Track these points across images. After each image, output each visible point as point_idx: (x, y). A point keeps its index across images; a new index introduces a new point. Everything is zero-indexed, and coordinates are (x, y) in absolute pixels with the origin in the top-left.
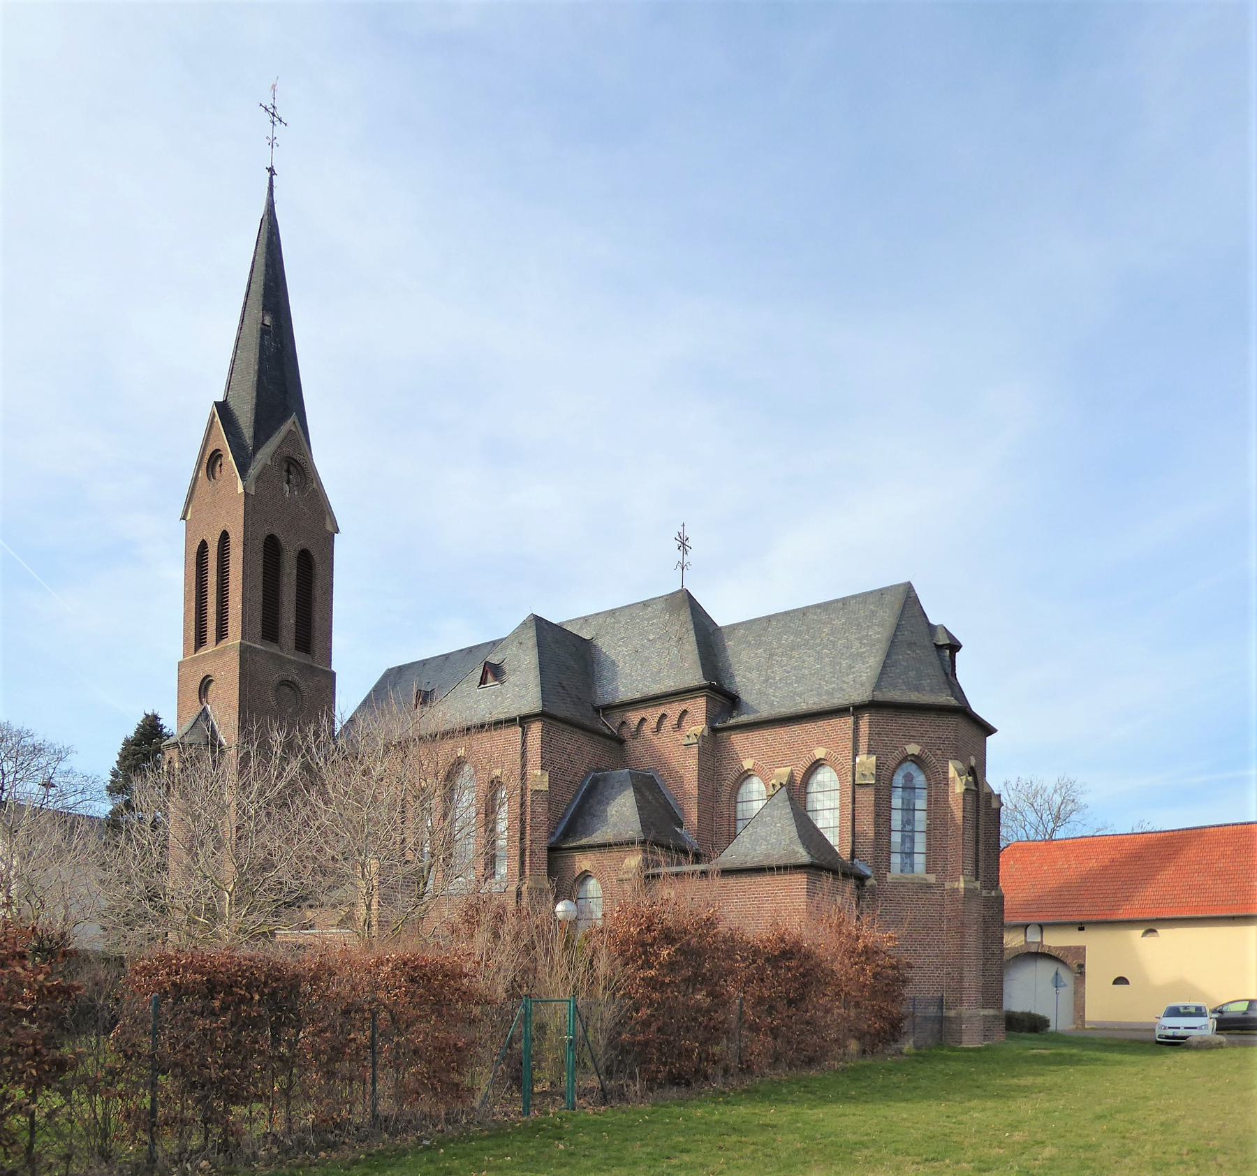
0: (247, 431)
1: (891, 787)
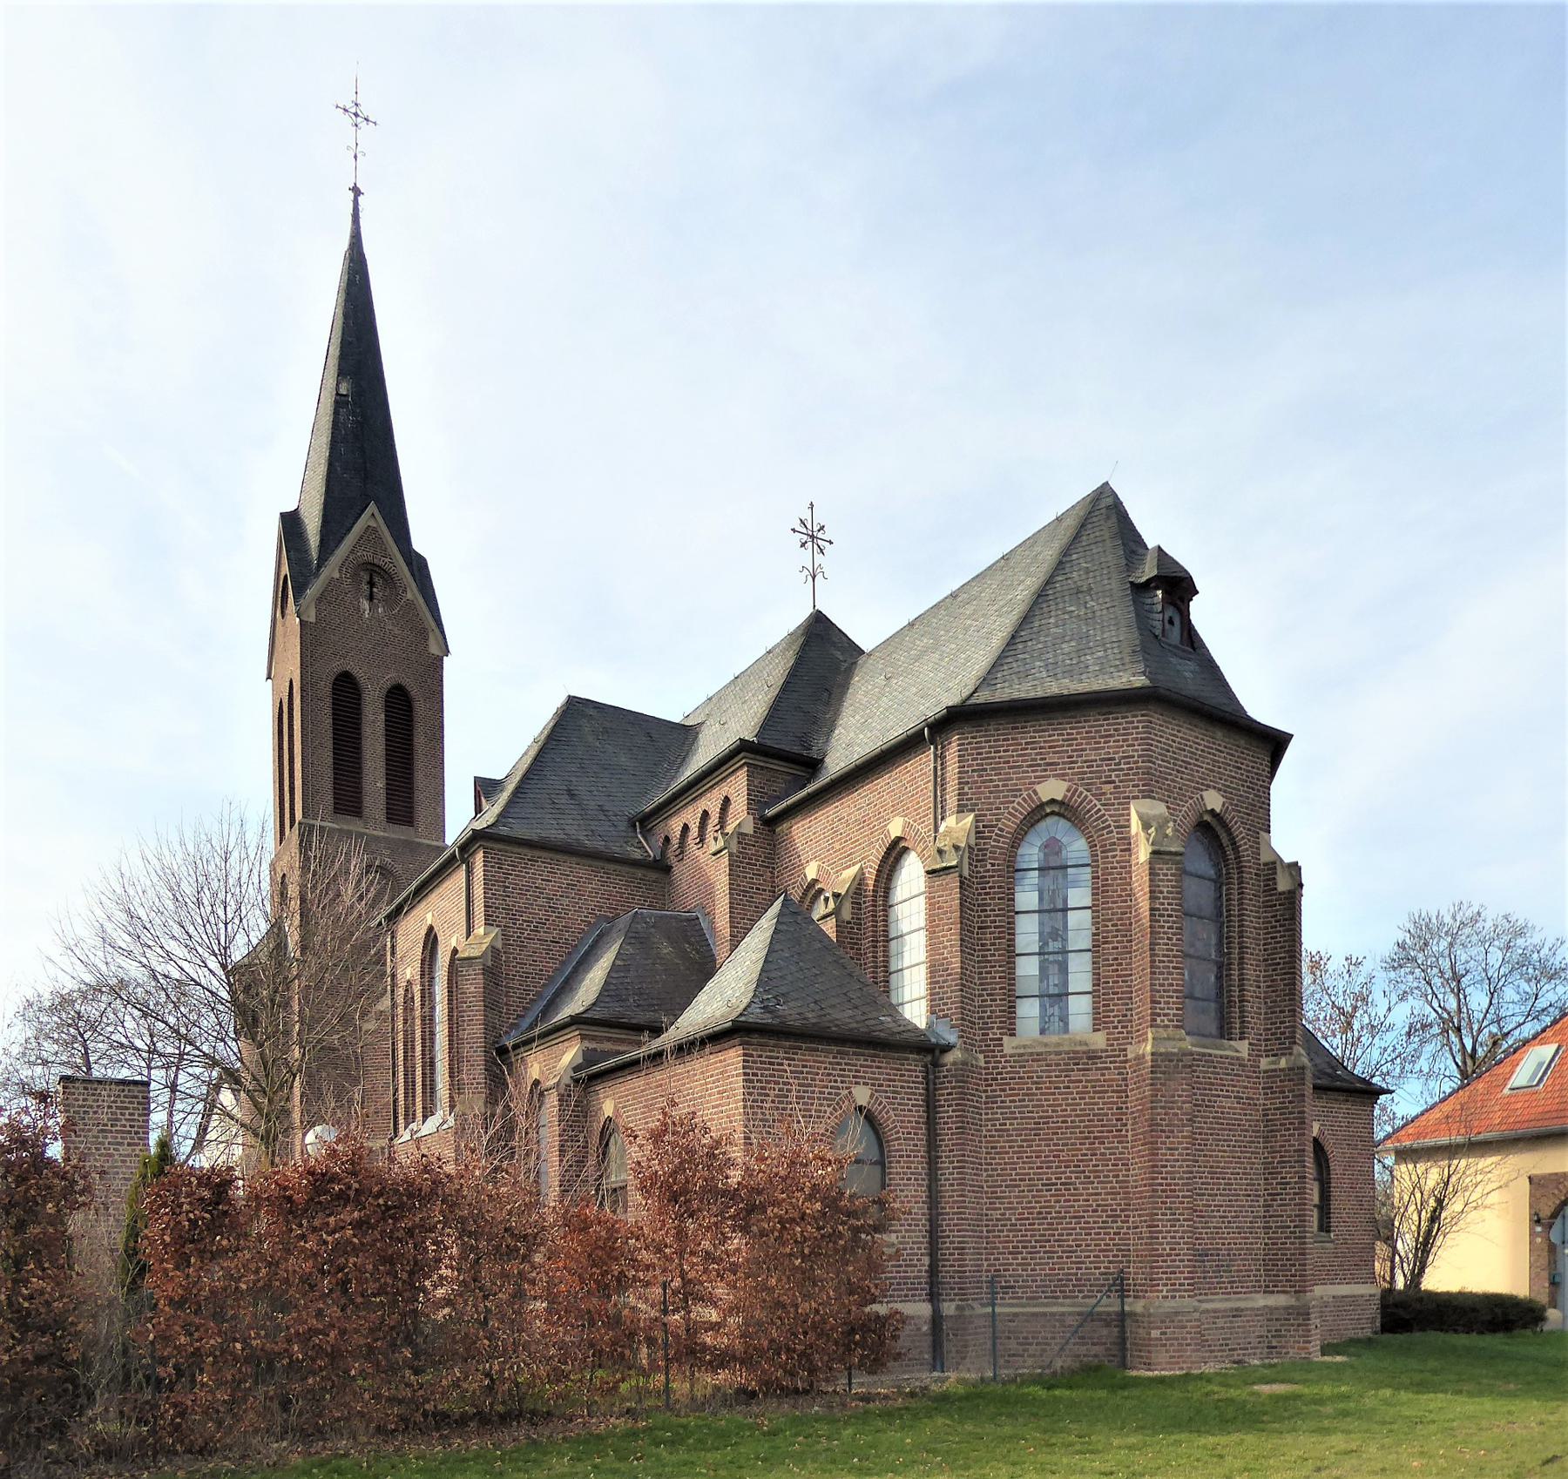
0: (314, 540)
1: (1012, 871)
